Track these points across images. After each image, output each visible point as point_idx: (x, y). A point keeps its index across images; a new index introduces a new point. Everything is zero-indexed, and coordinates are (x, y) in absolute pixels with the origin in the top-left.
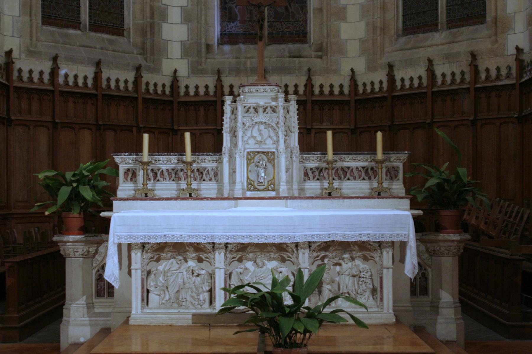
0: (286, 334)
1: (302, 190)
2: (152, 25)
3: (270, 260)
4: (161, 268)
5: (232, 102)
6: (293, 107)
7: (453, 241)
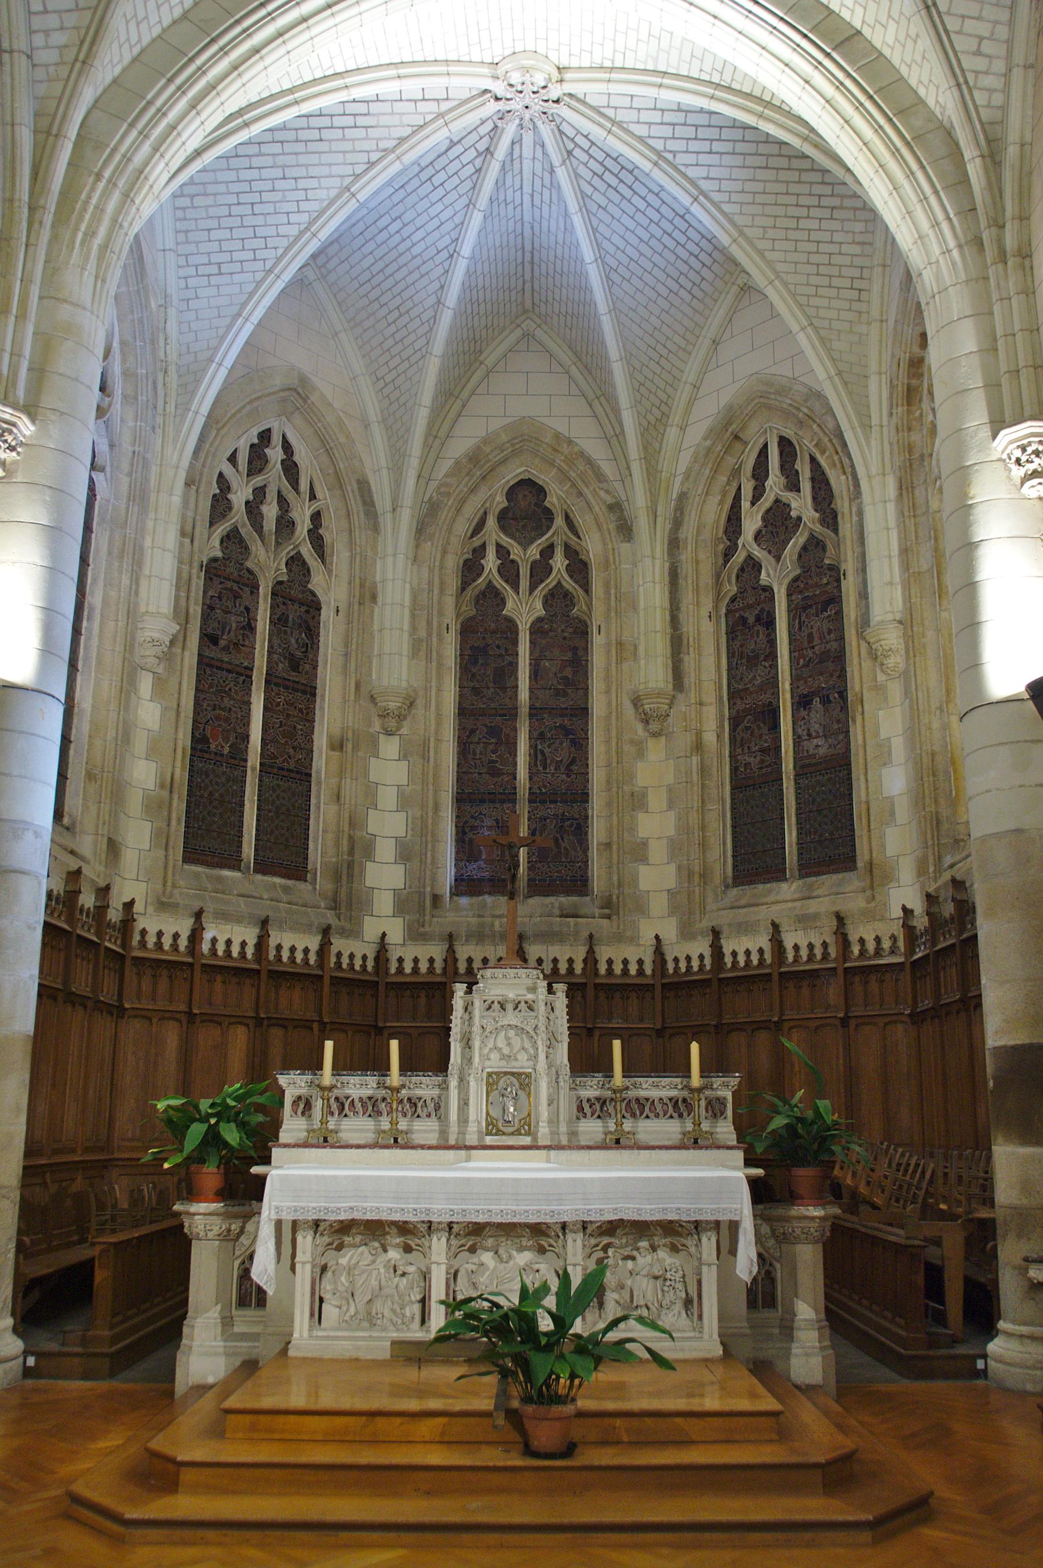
0: (541, 1381)
1: (573, 1134)
2: (350, 865)
3: (521, 1249)
4: (343, 1261)
5: (466, 993)
6: (561, 1001)
7: (813, 1218)
